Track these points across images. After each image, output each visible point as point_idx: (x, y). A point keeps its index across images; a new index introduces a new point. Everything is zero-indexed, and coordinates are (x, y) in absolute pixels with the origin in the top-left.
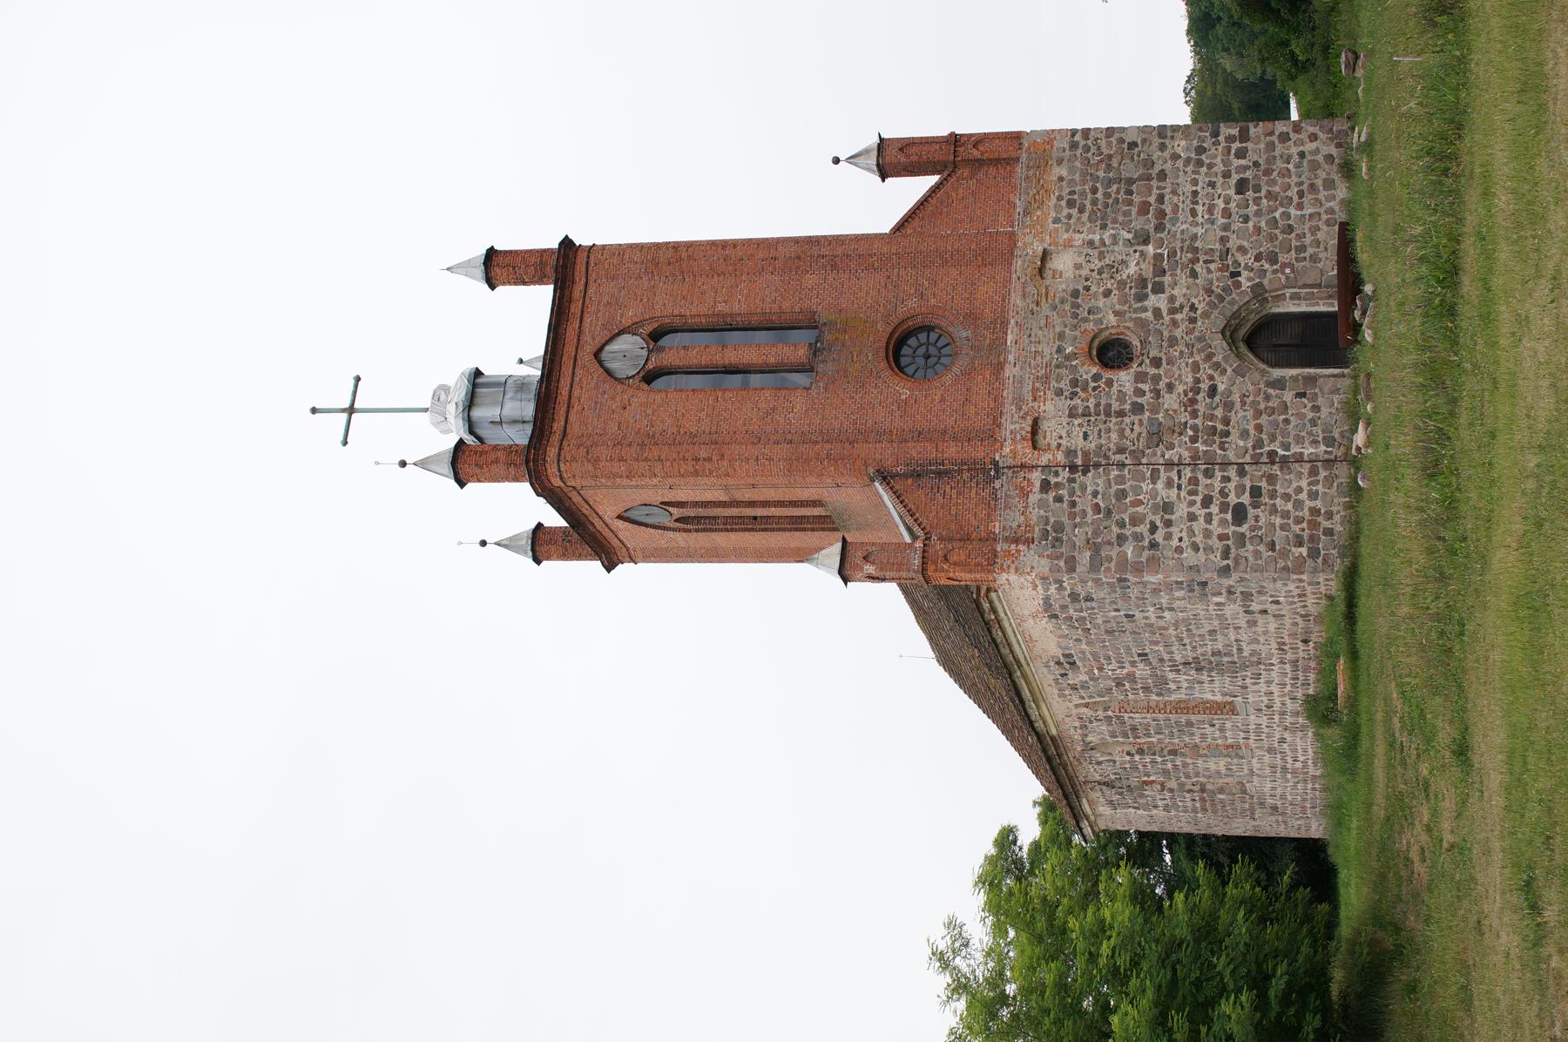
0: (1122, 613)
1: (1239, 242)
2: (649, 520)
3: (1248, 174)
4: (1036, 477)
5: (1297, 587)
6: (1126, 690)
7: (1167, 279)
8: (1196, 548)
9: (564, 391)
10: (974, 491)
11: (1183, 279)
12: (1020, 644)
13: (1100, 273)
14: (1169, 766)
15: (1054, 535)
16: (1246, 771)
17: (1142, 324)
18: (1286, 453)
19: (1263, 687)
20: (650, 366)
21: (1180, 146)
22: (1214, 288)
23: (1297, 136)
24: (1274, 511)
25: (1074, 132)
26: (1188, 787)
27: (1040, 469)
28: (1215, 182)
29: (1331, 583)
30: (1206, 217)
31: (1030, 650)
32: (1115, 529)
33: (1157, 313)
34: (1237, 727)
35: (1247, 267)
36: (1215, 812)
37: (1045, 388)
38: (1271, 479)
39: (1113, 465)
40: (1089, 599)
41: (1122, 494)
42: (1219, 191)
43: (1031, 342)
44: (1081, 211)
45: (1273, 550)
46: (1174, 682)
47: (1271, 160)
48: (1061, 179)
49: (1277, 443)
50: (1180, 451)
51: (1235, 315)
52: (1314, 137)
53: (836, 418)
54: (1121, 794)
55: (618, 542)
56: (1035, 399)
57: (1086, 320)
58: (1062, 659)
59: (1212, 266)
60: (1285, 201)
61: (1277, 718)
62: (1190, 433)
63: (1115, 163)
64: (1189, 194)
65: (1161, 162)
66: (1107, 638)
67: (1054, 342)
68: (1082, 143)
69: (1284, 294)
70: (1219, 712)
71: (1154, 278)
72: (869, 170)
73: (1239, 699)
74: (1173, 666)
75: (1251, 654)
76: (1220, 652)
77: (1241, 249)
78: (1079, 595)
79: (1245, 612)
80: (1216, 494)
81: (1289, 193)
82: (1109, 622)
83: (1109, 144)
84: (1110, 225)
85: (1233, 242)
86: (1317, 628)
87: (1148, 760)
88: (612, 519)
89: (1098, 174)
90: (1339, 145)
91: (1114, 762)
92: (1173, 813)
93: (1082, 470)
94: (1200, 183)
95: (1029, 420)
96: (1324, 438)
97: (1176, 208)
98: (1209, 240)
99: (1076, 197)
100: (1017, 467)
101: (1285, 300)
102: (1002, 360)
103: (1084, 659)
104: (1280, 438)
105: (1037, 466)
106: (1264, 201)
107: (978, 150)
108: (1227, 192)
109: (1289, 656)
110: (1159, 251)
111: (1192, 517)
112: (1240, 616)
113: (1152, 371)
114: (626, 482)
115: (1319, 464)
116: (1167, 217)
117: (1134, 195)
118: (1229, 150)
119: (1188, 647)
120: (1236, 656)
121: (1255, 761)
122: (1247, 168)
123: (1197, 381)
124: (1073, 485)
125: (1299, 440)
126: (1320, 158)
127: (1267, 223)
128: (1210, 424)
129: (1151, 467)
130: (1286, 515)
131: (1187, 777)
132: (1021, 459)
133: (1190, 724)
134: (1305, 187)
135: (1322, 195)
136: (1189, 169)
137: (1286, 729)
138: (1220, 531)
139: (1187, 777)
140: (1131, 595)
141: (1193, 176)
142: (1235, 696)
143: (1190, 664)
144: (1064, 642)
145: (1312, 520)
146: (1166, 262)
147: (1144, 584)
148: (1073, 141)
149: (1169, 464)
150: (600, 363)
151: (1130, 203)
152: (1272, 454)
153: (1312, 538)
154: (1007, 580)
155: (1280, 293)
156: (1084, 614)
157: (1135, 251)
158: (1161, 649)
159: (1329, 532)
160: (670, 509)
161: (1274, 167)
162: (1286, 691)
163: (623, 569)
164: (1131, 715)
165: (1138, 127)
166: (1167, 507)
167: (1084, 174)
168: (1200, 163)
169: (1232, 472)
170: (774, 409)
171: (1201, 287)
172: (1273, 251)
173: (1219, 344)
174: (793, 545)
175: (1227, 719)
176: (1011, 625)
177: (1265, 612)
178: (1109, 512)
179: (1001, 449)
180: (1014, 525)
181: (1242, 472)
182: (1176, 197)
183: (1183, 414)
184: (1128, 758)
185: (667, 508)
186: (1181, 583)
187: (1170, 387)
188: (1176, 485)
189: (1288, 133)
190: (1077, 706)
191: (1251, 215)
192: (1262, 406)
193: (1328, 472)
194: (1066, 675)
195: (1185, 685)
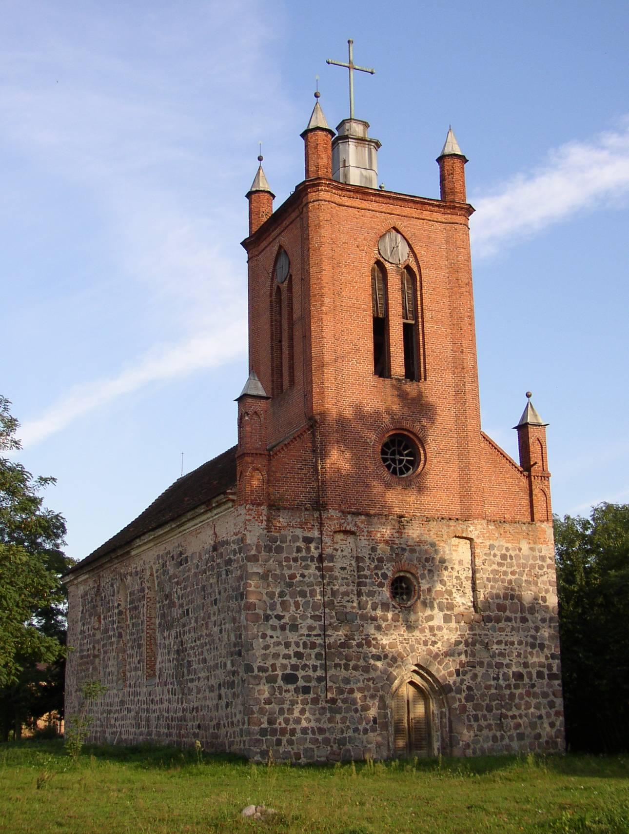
0: (218, 597)
4: (316, 534)
5: (238, 721)
6: (163, 602)
8: (267, 647)
10: (304, 490)
14: (111, 633)
23: (553, 714)
27: (320, 536)
29: (242, 744)
30: (497, 651)
32: (277, 591)
35: (462, 681)
39: (324, 588)
44: (500, 564)
47: (535, 695)
61: (145, 707)
69: (444, 707)
70: (148, 666)
72: (525, 415)
73: (157, 681)
75: (189, 688)
77: (475, 676)
78: (231, 565)
79: (220, 685)
80: (304, 662)
83: (544, 583)
90: (547, 742)
91: (113, 596)
92: (80, 637)
97: (502, 630)
99: (509, 560)
103: (184, 571)
106: (508, 692)
108: (514, 666)
116: (496, 624)
117: (511, 601)
118: (544, 667)
119: (194, 644)
121: (115, 691)
122: (531, 679)
129: (323, 615)
130: (290, 710)
131: (104, 646)
136: (530, 640)
141: (524, 642)
143: (182, 645)
147: (239, 612)
153: (274, 732)
154: (241, 514)
155: (446, 704)
158: (192, 625)
161: (532, 698)
164: (146, 605)
166: (294, 628)
167: (524, 566)
172: (474, 698)
177: (220, 697)
182: (510, 630)
184: (116, 605)
186: (240, 638)
188: (310, 633)
190: (151, 568)
194: (173, 560)
195: (167, 642)
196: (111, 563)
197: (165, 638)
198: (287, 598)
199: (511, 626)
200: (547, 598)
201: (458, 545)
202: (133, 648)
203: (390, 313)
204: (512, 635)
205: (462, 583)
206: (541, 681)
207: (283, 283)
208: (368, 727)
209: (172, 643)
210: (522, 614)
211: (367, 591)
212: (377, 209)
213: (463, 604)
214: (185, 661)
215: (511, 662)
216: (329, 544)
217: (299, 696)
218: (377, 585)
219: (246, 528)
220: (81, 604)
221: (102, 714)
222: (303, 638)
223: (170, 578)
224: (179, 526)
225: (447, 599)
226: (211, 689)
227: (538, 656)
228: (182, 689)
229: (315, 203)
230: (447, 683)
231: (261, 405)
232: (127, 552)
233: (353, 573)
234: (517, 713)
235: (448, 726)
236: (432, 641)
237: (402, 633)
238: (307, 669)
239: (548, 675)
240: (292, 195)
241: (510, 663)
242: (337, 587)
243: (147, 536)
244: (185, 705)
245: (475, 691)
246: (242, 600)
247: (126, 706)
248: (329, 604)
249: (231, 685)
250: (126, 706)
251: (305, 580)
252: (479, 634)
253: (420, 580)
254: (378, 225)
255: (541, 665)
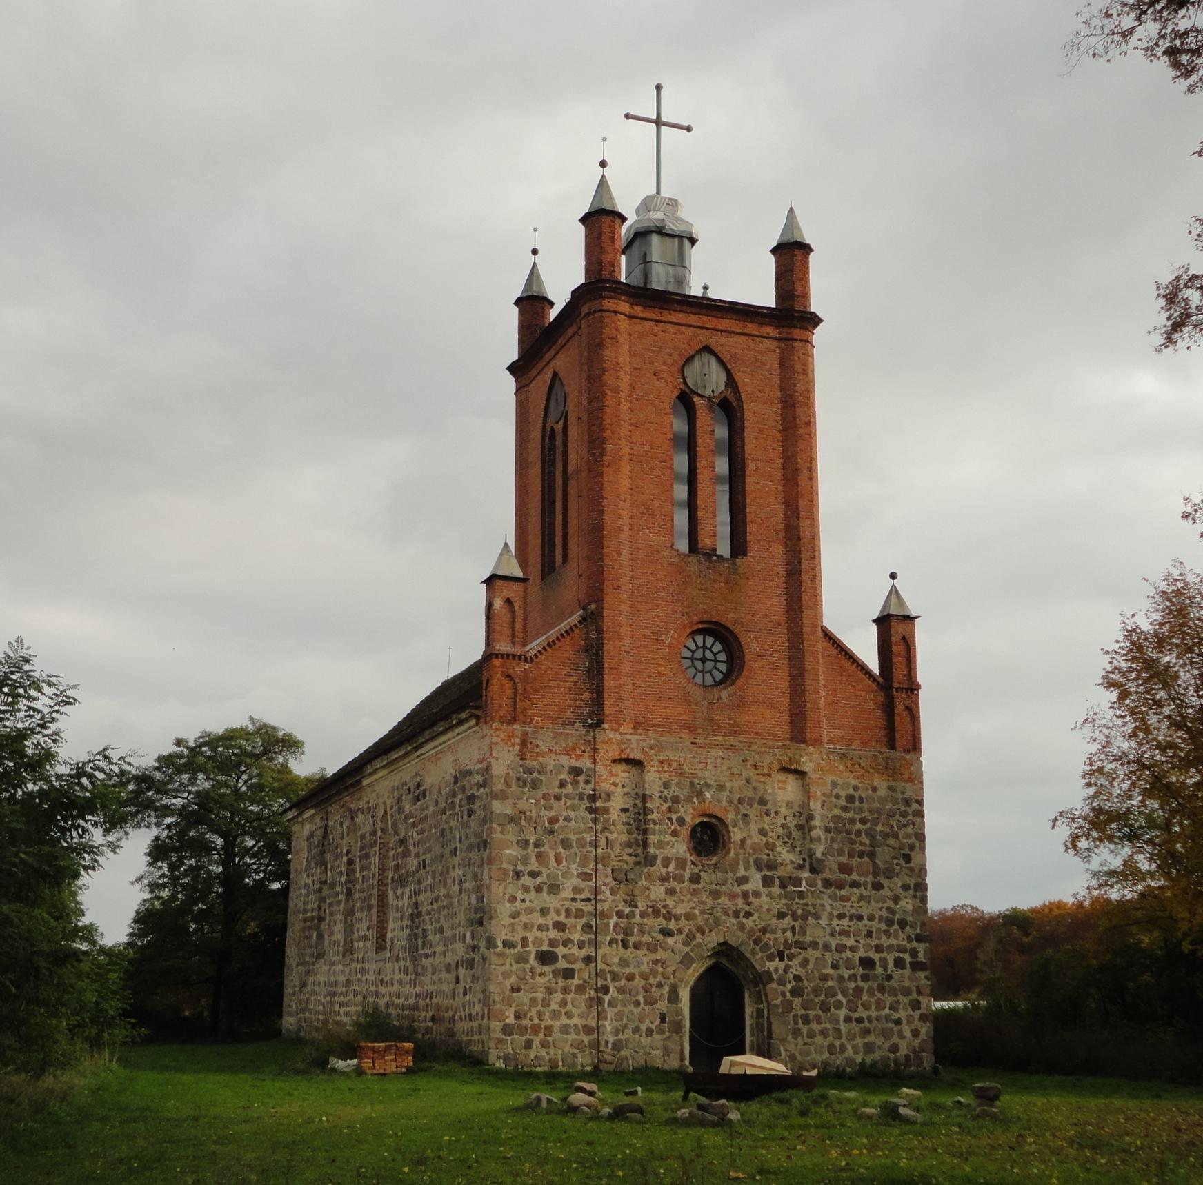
0: (458, 845)
1: (812, 961)
2: (552, 403)
3: (879, 970)
4: (585, 763)
5: (477, 1014)
6: (396, 849)
7: (776, 890)
8: (514, 915)
9: (669, 317)
10: (572, 703)
11: (780, 905)
12: (434, 748)
13: (783, 825)
14: (338, 889)
15: (529, 779)
16: (333, 959)
17: (734, 867)
18: (606, 1005)
19: (397, 977)
20: (696, 399)
21: (907, 904)
22: (768, 935)
23: (917, 1017)
24: (550, 991)
25: (920, 803)
26: (322, 904)
27: (592, 766)
28: (871, 937)
29: (481, 1045)
30: (838, 928)
31: (429, 758)
32: (533, 839)
33: (743, 880)
34: (367, 952)
35: (787, 968)
36: (304, 929)
37: (671, 772)
38: (580, 989)
39: (596, 836)
40: (470, 813)
41: (566, 844)
42: (862, 942)
43: (716, 759)
44: (845, 809)
45: (513, 990)
46: (403, 894)
47: (893, 992)
48: (874, 789)
49: (616, 994)
50: (610, 900)
51: (741, 956)
52: (915, 1033)
53: (643, 574)
54: (318, 846)
55: (534, 375)
56: (661, 762)
57: (737, 811)
58: (422, 788)
59: (789, 934)
60: (852, 1005)
61: (373, 989)
62: (627, 910)
63: (891, 841)
64: (860, 913)
65: (892, 886)
66: (438, 830)
67: (715, 781)
68: (910, 810)
69: (762, 1003)
70: (379, 935)
71: (778, 878)
72: (886, 605)
73: (388, 955)
74: (415, 892)
75: (423, 966)
76: (426, 937)
77: (805, 963)
78: (473, 804)
79: (458, 962)
80: (566, 935)
81: (860, 1009)
82: (451, 832)
83: (908, 836)
84: (830, 835)
85: (812, 954)
86: (443, 1030)
87: (343, 869)
88: (553, 368)
89: (880, 824)
90: (907, 1057)
91: (342, 839)
92: (303, 892)
93: (591, 807)
94: (870, 923)
95: (639, 757)
96: (621, 1041)
97: (845, 899)
98: (817, 931)
99: (857, 803)
100: (595, 745)
101: (756, 1003)
102: (700, 731)
103: (423, 810)
104: (621, 997)
105: (595, 763)
106: (853, 985)
107: (903, 711)
108: (862, 949)
109: (422, 1002)
110: (804, 882)
111: (544, 912)
112: (455, 957)
113: (687, 875)
114: (584, 375)
115: (596, 1035)
116: (838, 892)
117: (859, 860)
118: (904, 951)
119: (430, 907)
120: (422, 952)
121: (340, 967)
122: (885, 969)
123: (677, 918)
124: (577, 798)
125: (619, 1016)
126: (895, 1039)
127: (832, 987)
128: (635, 930)
129: (593, 873)
130: (546, 1003)
131: (330, 905)
132: (603, 749)
133: (370, 908)
134: (867, 1024)
135: (859, 1041)
136: (885, 913)
137: (364, 997)
138: (531, 939)
139: (330, 905)
140: (473, 853)
141: (877, 917)
142: (390, 951)
143: (417, 908)
144: (435, 791)
145: (541, 1028)
146: (793, 889)
147: (481, 866)
148: (911, 801)
149: (596, 891)
150: (699, 352)
151: (851, 855)
152: (606, 990)
153: (522, 1030)
154: (486, 735)
155: (764, 999)
156: (457, 808)
157: (804, 860)
158: (429, 882)
159: (528, 1045)
160: (562, 422)
161: (886, 995)
162: (394, 998)
163: (510, 382)
164: (378, 853)
165: (925, 865)
166: (554, 889)
167: (879, 812)
168: (890, 923)
169: (588, 951)
170: (652, 515)
171: (768, 922)
172: (804, 992)
173: (712, 940)
174: (530, 538)
175: (373, 942)
176: (449, 740)
177: (457, 981)
178: (551, 832)
179: (612, 730)
180: (540, 743)
181: (588, 960)
182: (856, 900)
183: (645, 904)
184: (345, 851)
185: (563, 418)
186: (482, 901)
187: (670, 892)
188: (576, 897)
189: (919, 1008)
190: (385, 803)
191: (839, 971)
192: (652, 980)
193: (587, 1044)
194: (409, 793)
195: (400, 904)
196: (340, 795)
197: (398, 897)
198: (546, 848)
199: (858, 895)
200: (912, 857)
201: (786, 781)
202: (362, 910)
203: (698, 464)
204: (861, 907)
205: (790, 832)
206: (900, 972)
207: (557, 423)
208: (653, 1027)
209: (406, 905)
210: (875, 877)
211: (656, 841)
212: (682, 322)
213: (792, 862)
214: (420, 930)
215: (858, 944)
216: (605, 777)
217: (559, 981)
218: (671, 834)
219: (491, 755)
220: (306, 848)
221: (325, 997)
222: (565, 902)
223: (405, 818)
224: (416, 749)
225: (768, 855)
226: (448, 968)
227: (897, 938)
228: (415, 967)
229: (596, 315)
230: (766, 969)
231: (514, 591)
232: (357, 781)
233: (637, 816)
234: (864, 1015)
235: (766, 1029)
236: (746, 912)
237: (704, 899)
238: (570, 945)
239: (910, 963)
240: (567, 304)
241: (857, 946)
242: (615, 835)
243: (379, 760)
244: (418, 989)
245: (805, 982)
246: (485, 850)
247: (352, 988)
248: (603, 858)
249: (470, 964)
250: (352, 988)
251: (570, 824)
252: (813, 904)
253: (731, 828)
254: (684, 344)
255: (902, 949)
